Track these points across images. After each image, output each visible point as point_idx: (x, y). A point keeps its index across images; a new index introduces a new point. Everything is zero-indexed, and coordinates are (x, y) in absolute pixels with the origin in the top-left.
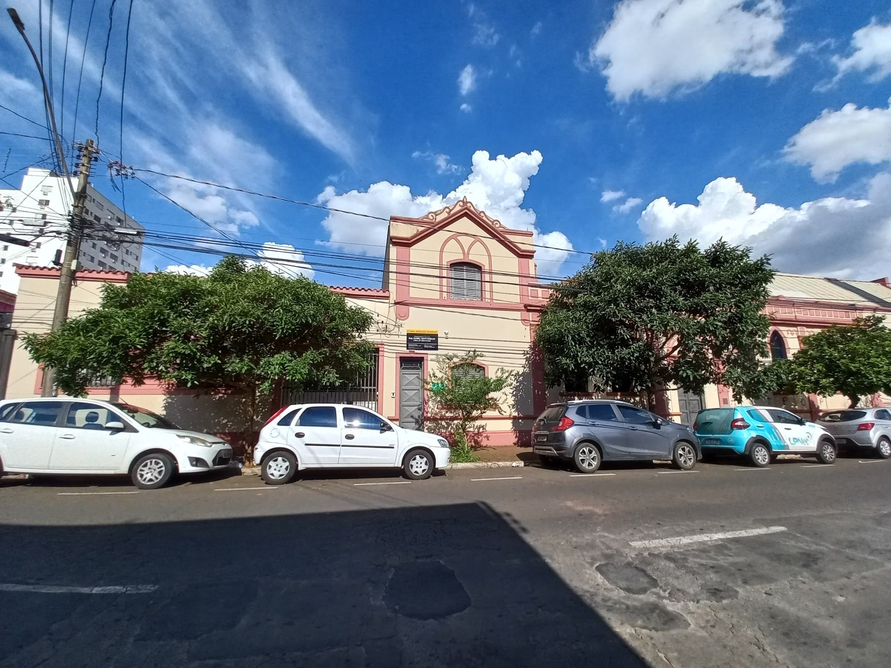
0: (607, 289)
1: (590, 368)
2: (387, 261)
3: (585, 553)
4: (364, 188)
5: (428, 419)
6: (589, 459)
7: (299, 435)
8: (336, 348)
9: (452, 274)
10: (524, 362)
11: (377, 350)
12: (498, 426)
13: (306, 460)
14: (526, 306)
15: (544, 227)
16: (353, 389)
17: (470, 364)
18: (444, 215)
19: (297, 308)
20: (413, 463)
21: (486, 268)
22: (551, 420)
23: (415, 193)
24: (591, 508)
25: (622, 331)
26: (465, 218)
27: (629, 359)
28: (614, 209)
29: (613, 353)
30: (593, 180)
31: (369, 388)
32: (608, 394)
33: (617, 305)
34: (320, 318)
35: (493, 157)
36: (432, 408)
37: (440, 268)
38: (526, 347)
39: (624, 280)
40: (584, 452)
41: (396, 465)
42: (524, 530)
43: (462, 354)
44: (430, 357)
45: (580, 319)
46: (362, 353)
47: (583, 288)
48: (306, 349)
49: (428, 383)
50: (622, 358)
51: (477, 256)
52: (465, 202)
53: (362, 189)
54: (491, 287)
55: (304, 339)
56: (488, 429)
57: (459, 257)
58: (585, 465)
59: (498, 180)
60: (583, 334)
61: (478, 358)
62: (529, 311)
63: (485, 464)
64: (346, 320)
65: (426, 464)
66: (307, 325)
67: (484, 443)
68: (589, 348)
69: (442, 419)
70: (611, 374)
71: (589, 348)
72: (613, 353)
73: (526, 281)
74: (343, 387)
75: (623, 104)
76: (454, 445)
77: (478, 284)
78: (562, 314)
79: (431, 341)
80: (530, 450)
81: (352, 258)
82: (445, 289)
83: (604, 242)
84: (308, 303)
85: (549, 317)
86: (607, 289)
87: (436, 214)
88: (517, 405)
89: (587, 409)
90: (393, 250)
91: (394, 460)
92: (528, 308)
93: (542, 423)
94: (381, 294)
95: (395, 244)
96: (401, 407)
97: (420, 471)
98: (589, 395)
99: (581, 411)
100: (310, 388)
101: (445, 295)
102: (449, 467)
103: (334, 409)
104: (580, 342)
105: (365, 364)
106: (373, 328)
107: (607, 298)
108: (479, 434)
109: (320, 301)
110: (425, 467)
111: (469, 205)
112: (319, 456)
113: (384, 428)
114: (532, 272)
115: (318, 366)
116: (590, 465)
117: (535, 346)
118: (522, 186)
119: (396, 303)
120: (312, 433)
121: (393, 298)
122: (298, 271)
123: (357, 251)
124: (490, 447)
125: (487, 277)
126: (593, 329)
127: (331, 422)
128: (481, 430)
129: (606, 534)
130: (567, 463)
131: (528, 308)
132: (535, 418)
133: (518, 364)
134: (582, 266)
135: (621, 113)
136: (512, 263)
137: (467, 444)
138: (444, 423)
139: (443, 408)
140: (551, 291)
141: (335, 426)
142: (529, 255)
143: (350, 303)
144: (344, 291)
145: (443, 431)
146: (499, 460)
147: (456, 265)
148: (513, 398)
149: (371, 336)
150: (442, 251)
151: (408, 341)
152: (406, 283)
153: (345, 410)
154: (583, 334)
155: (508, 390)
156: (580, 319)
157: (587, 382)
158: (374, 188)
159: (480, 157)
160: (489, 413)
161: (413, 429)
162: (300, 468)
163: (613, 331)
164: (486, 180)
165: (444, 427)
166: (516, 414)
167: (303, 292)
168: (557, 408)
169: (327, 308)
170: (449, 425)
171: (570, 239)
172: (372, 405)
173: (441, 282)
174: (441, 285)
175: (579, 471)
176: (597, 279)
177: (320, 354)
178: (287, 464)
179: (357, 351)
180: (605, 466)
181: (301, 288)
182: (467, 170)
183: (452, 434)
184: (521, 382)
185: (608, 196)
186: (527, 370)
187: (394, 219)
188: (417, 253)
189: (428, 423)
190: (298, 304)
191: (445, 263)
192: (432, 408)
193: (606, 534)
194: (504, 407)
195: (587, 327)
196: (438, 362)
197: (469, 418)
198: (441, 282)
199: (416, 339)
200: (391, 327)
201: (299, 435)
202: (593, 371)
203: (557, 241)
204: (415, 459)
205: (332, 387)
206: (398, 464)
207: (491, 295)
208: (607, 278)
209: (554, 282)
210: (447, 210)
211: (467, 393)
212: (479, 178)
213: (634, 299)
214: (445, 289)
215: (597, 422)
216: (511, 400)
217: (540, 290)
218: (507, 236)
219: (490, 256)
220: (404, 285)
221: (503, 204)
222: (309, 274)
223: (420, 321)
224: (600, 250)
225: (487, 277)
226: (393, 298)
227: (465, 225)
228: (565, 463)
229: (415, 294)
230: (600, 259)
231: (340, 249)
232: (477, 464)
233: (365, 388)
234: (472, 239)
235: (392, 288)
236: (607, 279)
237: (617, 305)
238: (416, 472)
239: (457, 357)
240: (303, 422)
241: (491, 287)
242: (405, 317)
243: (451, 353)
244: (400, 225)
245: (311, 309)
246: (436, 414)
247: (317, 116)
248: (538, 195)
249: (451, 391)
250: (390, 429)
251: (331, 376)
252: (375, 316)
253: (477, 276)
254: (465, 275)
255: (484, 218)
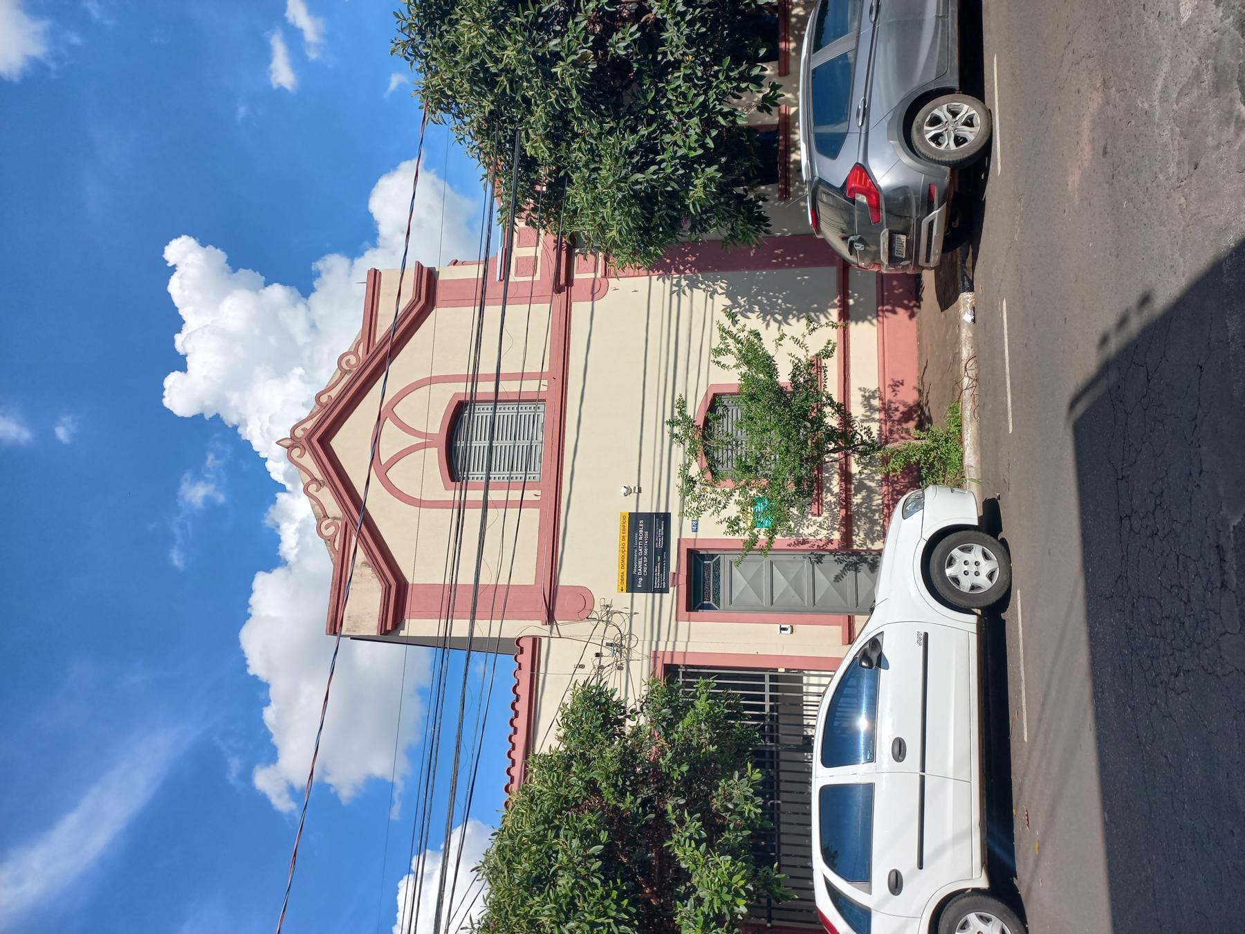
0: (514, 83)
1: (716, 125)
2: (443, 644)
3: (1210, 141)
4: (255, 692)
5: (847, 538)
6: (956, 124)
7: (896, 884)
8: (662, 782)
9: (477, 475)
10: (699, 294)
11: (671, 670)
12: (863, 360)
13: (962, 867)
14: (558, 289)
15: (360, 235)
16: (771, 732)
17: (705, 432)
18: (326, 495)
19: (564, 882)
20: (966, 584)
21: (462, 388)
22: (850, 224)
23: (271, 559)
24: (1086, 124)
25: (621, 43)
26: (336, 443)
27: (690, 24)
28: (313, 55)
29: (676, 65)
30: (242, 111)
31: (767, 693)
32: (784, 71)
33: (556, 56)
34: (588, 821)
35: (180, 364)
36: (818, 527)
37: (461, 506)
38: (660, 286)
39: (491, 39)
40: (936, 138)
41: (974, 628)
42: (1145, 300)
43: (679, 453)
44: (688, 534)
45: (591, 151)
46: (675, 711)
47: (512, 141)
48: (668, 859)
49: (754, 540)
50: (690, 42)
51: (429, 410)
52: (292, 444)
53: (262, 695)
54: (511, 377)
55: (645, 865)
56: (873, 384)
57: (434, 458)
58: (971, 134)
59: (240, 353)
60: (630, 141)
61: (690, 412)
62: (569, 281)
63: (967, 395)
64: (592, 754)
65: (967, 550)
66: (608, 857)
67: (908, 396)
68: (666, 127)
69: (846, 502)
70: (730, 69)
71: (666, 127)
72: (676, 65)
73: (495, 289)
74: (765, 760)
75: (53, 37)
76: (915, 476)
77: (504, 411)
78: (577, 196)
79: (648, 530)
80: (928, 278)
81: (436, 718)
82: (515, 495)
83: (395, 80)
84: (551, 853)
85: (586, 229)
86: (514, 83)
87: (322, 516)
88: (807, 308)
89: (824, 129)
90: (415, 626)
91: (958, 634)
92: (563, 284)
93: (859, 247)
94: (525, 659)
95: (398, 621)
96: (814, 610)
97: (986, 567)
98: (787, 123)
99: (828, 146)
100: (769, 849)
101: (530, 495)
102: (974, 487)
103: (826, 791)
104: (649, 150)
105: (701, 705)
106: (614, 682)
107: (537, 81)
108: (886, 409)
109: (547, 820)
110: (976, 554)
111: (299, 433)
112: (949, 834)
113: (872, 657)
114: (473, 272)
115: (713, 826)
116: (969, 123)
117: (660, 267)
118: (256, 290)
119: (551, 619)
120: (889, 846)
121: (534, 627)
122: (465, 875)
123: (415, 711)
124: (921, 380)
125: (486, 388)
126: (617, 118)
127: (859, 797)
128: (876, 403)
129: (1160, 82)
130: (966, 185)
131: (563, 284)
132: (845, 266)
133: (706, 307)
134: (455, 139)
135: (76, 40)
136: (448, 327)
137: (911, 442)
138: (857, 499)
139: (819, 501)
140: (521, 224)
141: (870, 788)
142: (429, 283)
143: (549, 740)
144: (518, 755)
145: (877, 500)
146: (956, 357)
147: (454, 468)
148: (793, 321)
149: (632, 686)
150: (420, 503)
151: (648, 588)
152: (501, 594)
153: (828, 761)
154: (630, 141)
155: (769, 336)
156: (591, 151)
157: (751, 130)
158: (256, 666)
159: (180, 395)
160: (832, 387)
161: (874, 582)
162: (982, 882)
163: (621, 65)
164: (239, 379)
165: (868, 499)
166: (834, 314)
167: (524, 865)
168: (820, 205)
169: (564, 804)
170: (861, 486)
171: (390, 166)
172: (812, 683)
173: (497, 505)
174: (506, 504)
175: (986, 149)
176: (488, 107)
177: (681, 822)
178: (972, 917)
179: (671, 724)
180: (972, 81)
181: (511, 870)
182: (213, 433)
183: (886, 478)
184: (752, 301)
185: (283, 74)
186: (721, 286)
187: (335, 626)
188: (423, 567)
189: (858, 539)
190: (552, 880)
191: (449, 495)
192: (818, 527)
193: (1160, 82)
194: (816, 343)
195: (611, 132)
196: (699, 511)
197: (845, 436)
198: (497, 505)
199: (641, 568)
200: (612, 634)
201: (896, 884)
202: (725, 116)
203: (392, 198)
204: (956, 580)
205: (768, 789)
206: (968, 624)
207: (532, 376)
208: (484, 79)
209: (496, 215)
210: (313, 488)
211: (783, 438)
212: (234, 398)
213: (539, 14)
214: (515, 495)
215: (858, 103)
216: (797, 327)
217: (517, 252)
218: (380, 334)
219: (431, 381)
220: (503, 600)
221: (301, 339)
222: (474, 842)
223: (594, 559)
224: (417, 100)
225: (486, 388)
226: (534, 627)
227: (351, 444)
228: (965, 189)
229: (526, 573)
230: (441, 99)
231: (410, 752)
232: (967, 414)
233: (767, 704)
234: (388, 425)
235: (512, 629)
236: (490, 81)
237: (556, 56)
238: (990, 576)
239: (687, 466)
240: (860, 872)
241: (511, 377)
242: (584, 598)
243: (677, 481)
244: (352, 608)
245: (568, 846)
246: (833, 517)
247: (70, 823)
248: (278, 247)
249: (775, 481)
250: (875, 643)
251: (738, 791)
252: (581, 678)
253: (483, 412)
254: (480, 443)
255: (334, 393)
